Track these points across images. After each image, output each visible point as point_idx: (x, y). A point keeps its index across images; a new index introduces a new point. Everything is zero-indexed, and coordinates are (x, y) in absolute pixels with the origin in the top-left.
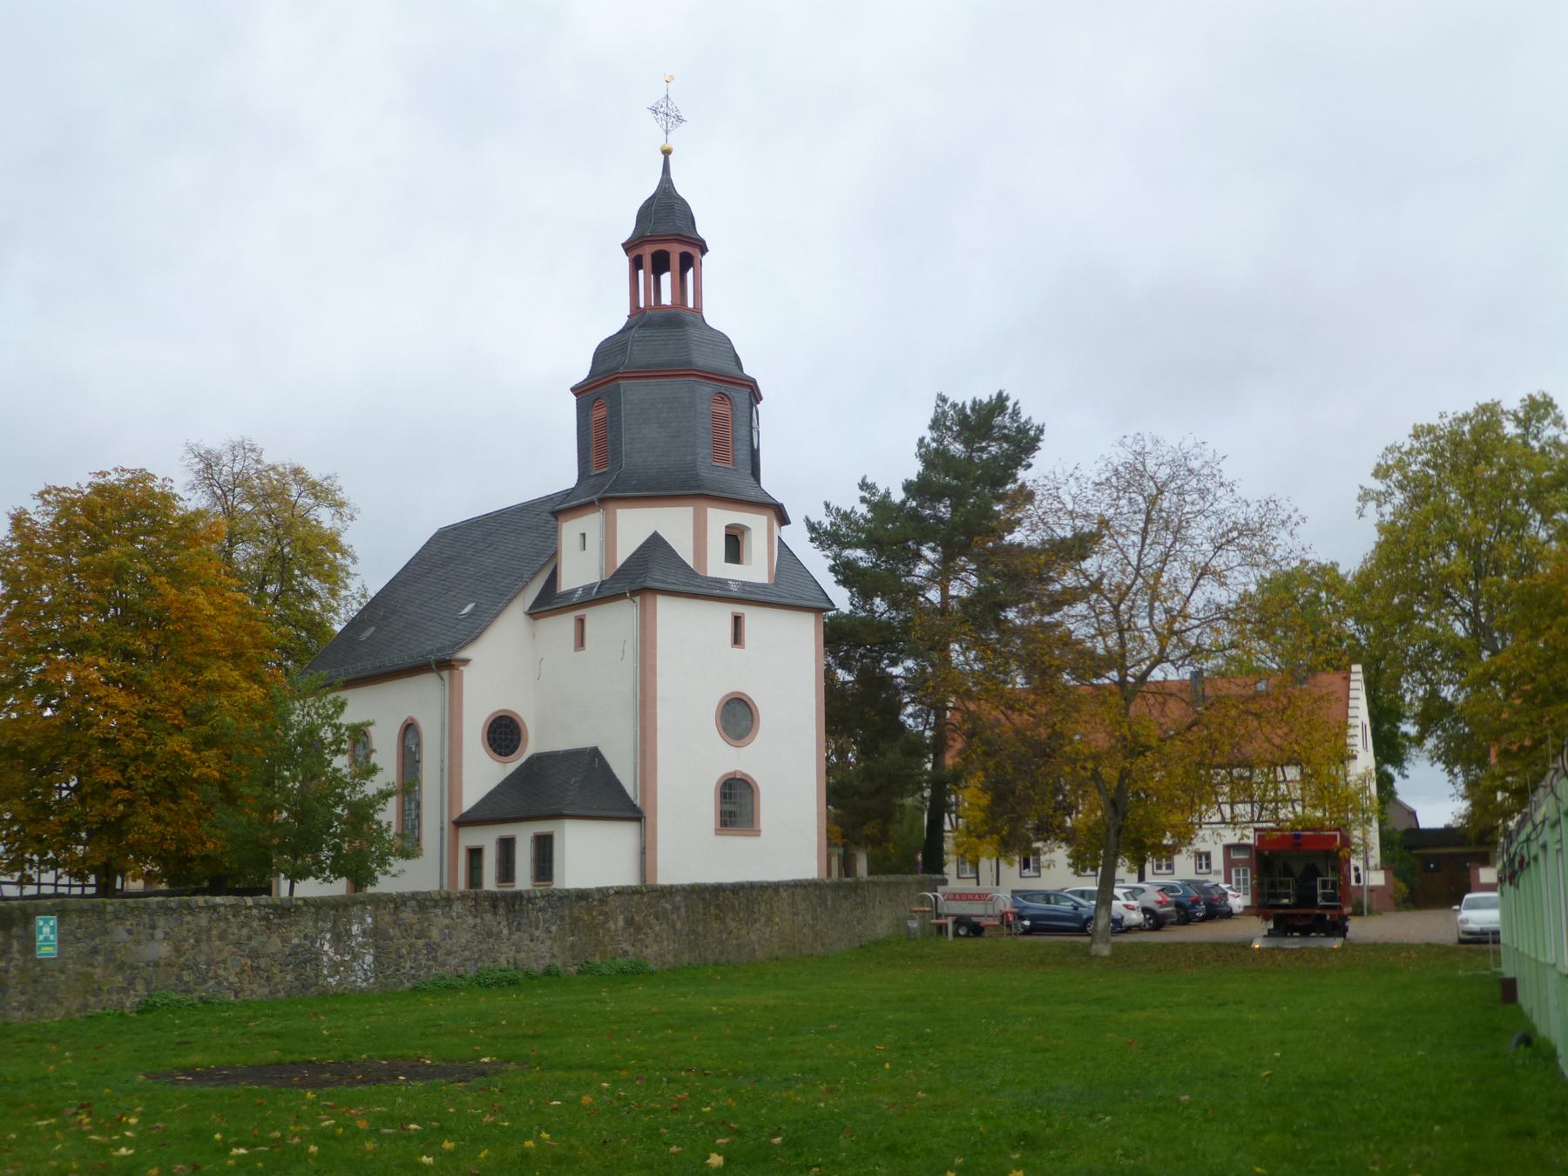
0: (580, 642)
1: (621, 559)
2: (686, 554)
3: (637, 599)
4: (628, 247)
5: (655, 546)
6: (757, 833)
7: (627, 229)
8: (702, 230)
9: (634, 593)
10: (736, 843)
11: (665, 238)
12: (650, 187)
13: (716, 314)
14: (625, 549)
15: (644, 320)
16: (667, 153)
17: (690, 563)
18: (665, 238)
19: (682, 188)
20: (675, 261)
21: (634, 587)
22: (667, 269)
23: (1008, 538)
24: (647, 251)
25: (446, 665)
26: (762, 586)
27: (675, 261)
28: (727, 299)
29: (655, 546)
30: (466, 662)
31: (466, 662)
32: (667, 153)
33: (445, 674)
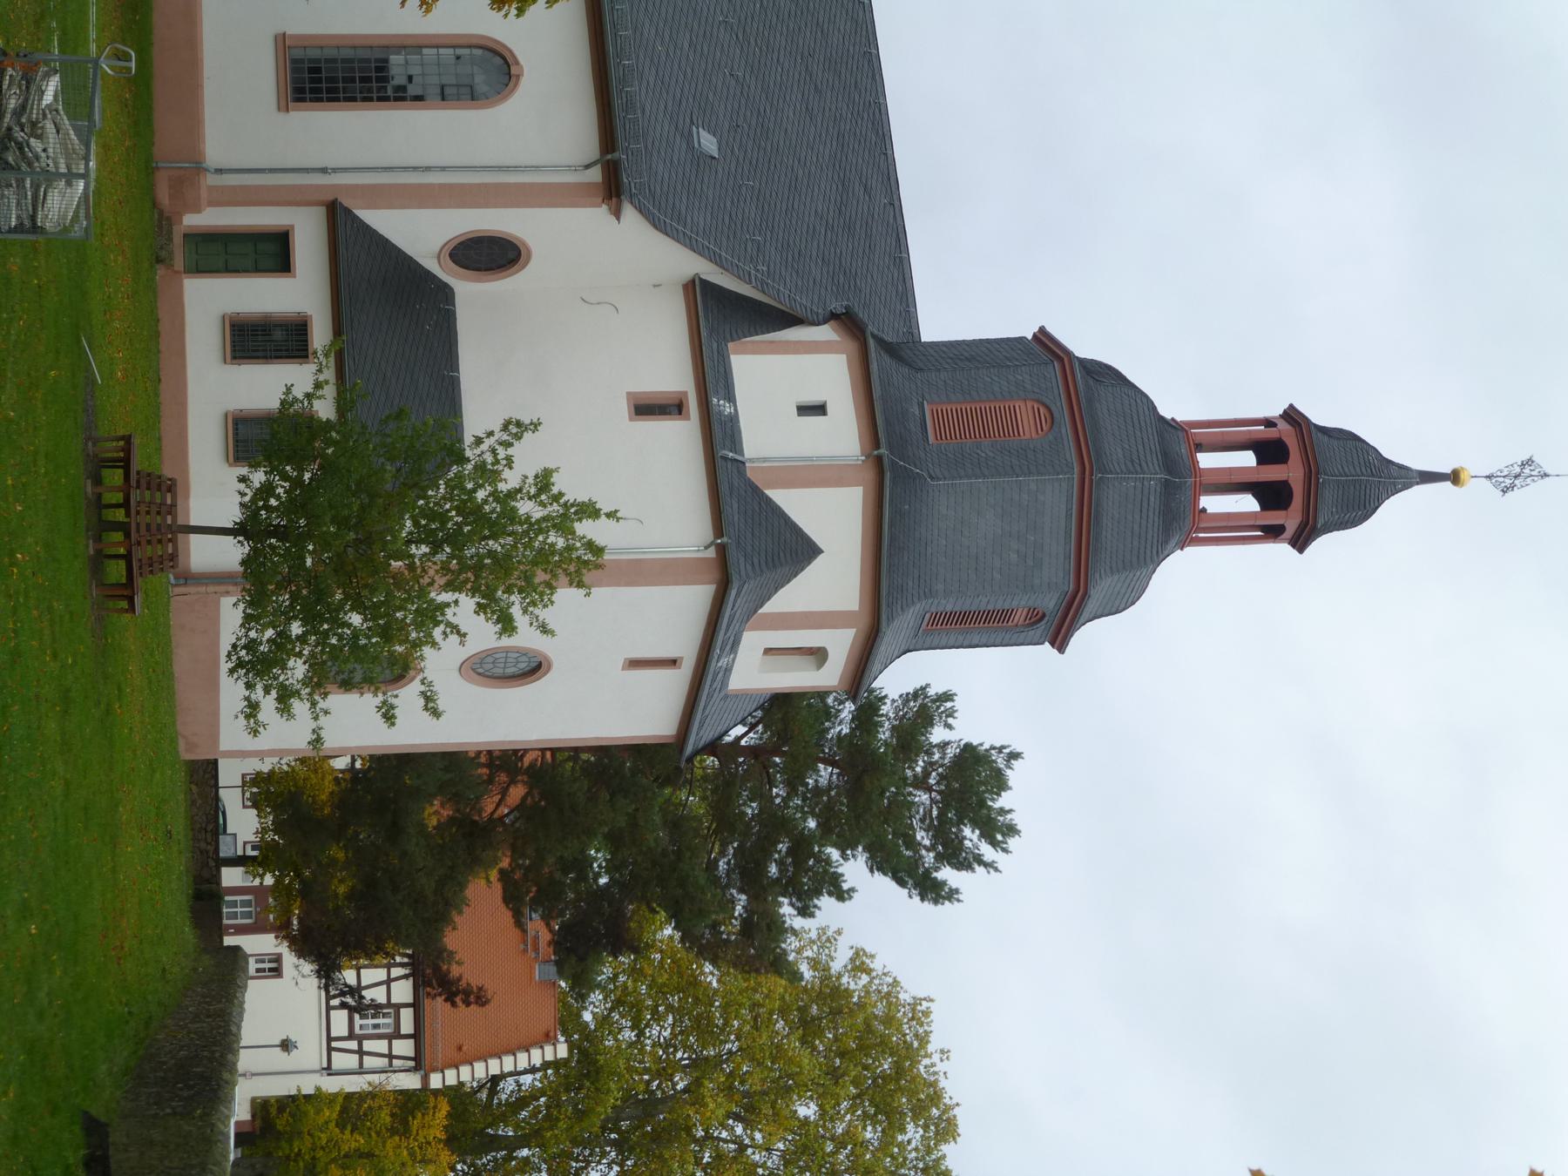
0: (646, 408)
1: (778, 496)
2: (781, 602)
3: (711, 553)
4: (1292, 416)
5: (796, 550)
6: (283, 107)
7: (1320, 415)
8: (1325, 545)
9: (722, 550)
10: (264, 75)
11: (1313, 480)
12: (1392, 449)
13: (1185, 574)
14: (796, 504)
15: (1176, 443)
16: (1454, 477)
17: (768, 608)
18: (1313, 480)
19: (1395, 510)
20: (1274, 473)
21: (733, 554)
22: (1264, 507)
23: (785, 901)
24: (1291, 473)
25: (613, 188)
26: (725, 683)
27: (1274, 518)
28: (1210, 594)
29: (796, 550)
30: (617, 214)
31: (617, 214)
32: (1454, 477)
33: (595, 175)
